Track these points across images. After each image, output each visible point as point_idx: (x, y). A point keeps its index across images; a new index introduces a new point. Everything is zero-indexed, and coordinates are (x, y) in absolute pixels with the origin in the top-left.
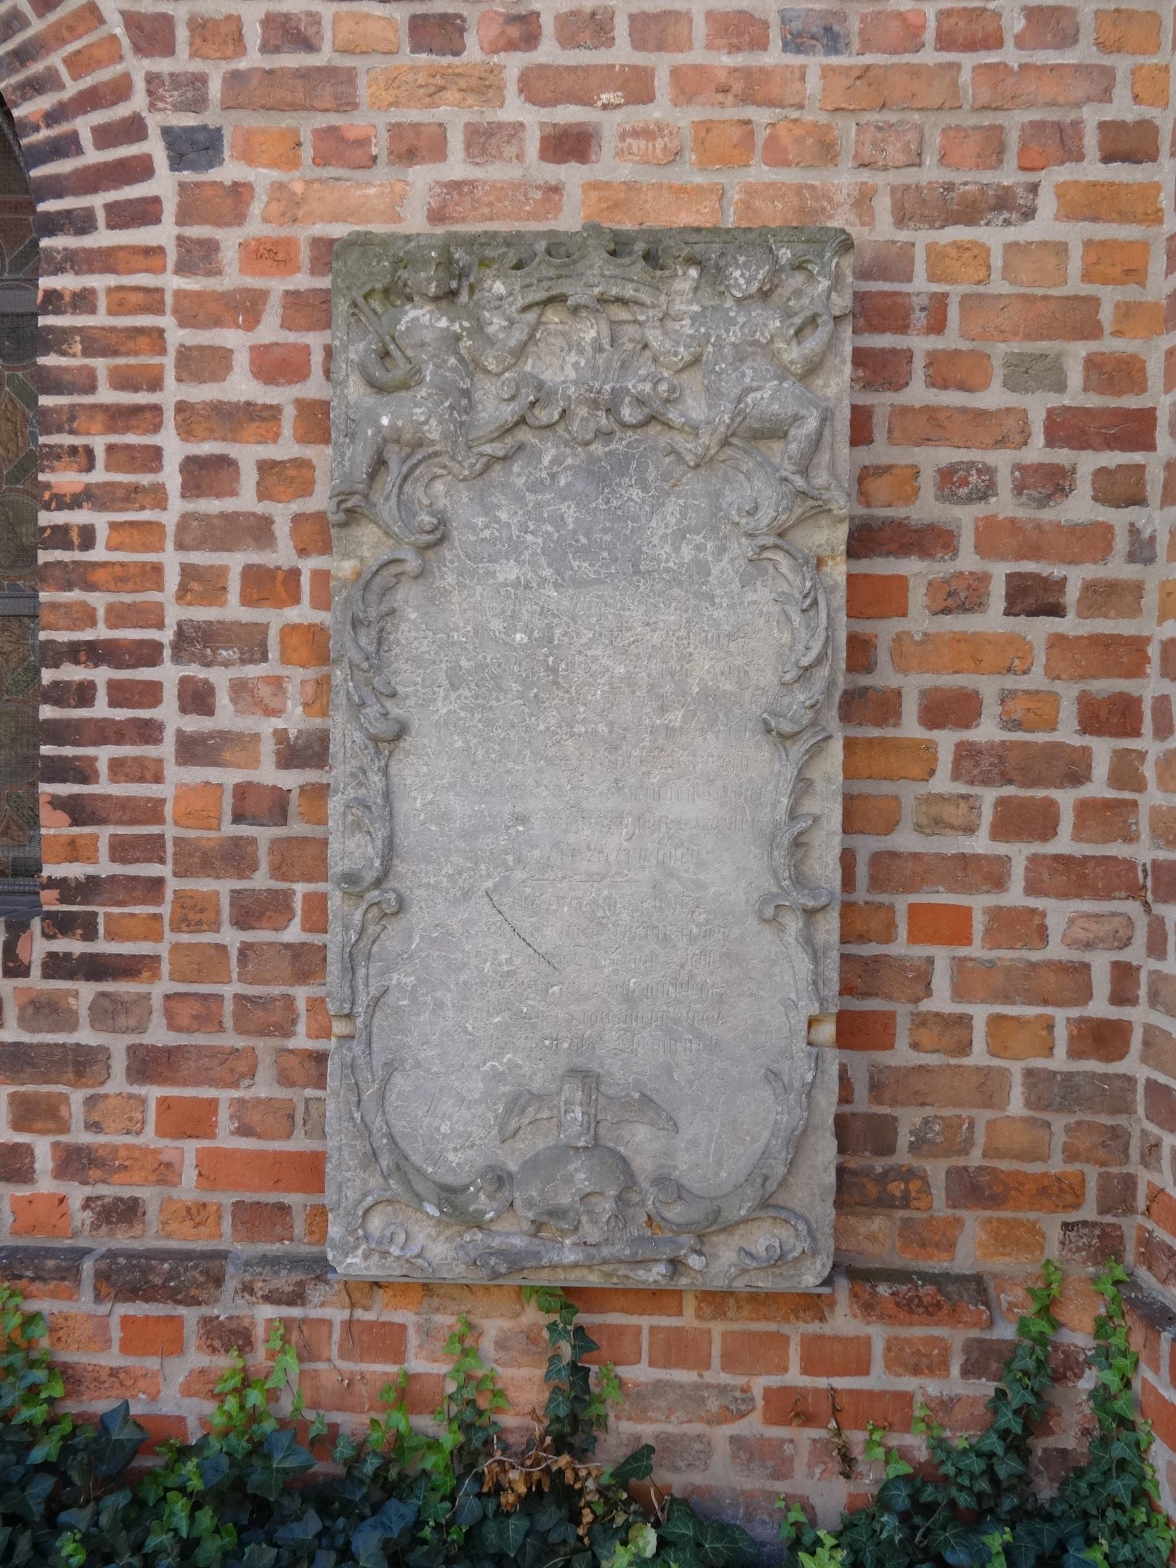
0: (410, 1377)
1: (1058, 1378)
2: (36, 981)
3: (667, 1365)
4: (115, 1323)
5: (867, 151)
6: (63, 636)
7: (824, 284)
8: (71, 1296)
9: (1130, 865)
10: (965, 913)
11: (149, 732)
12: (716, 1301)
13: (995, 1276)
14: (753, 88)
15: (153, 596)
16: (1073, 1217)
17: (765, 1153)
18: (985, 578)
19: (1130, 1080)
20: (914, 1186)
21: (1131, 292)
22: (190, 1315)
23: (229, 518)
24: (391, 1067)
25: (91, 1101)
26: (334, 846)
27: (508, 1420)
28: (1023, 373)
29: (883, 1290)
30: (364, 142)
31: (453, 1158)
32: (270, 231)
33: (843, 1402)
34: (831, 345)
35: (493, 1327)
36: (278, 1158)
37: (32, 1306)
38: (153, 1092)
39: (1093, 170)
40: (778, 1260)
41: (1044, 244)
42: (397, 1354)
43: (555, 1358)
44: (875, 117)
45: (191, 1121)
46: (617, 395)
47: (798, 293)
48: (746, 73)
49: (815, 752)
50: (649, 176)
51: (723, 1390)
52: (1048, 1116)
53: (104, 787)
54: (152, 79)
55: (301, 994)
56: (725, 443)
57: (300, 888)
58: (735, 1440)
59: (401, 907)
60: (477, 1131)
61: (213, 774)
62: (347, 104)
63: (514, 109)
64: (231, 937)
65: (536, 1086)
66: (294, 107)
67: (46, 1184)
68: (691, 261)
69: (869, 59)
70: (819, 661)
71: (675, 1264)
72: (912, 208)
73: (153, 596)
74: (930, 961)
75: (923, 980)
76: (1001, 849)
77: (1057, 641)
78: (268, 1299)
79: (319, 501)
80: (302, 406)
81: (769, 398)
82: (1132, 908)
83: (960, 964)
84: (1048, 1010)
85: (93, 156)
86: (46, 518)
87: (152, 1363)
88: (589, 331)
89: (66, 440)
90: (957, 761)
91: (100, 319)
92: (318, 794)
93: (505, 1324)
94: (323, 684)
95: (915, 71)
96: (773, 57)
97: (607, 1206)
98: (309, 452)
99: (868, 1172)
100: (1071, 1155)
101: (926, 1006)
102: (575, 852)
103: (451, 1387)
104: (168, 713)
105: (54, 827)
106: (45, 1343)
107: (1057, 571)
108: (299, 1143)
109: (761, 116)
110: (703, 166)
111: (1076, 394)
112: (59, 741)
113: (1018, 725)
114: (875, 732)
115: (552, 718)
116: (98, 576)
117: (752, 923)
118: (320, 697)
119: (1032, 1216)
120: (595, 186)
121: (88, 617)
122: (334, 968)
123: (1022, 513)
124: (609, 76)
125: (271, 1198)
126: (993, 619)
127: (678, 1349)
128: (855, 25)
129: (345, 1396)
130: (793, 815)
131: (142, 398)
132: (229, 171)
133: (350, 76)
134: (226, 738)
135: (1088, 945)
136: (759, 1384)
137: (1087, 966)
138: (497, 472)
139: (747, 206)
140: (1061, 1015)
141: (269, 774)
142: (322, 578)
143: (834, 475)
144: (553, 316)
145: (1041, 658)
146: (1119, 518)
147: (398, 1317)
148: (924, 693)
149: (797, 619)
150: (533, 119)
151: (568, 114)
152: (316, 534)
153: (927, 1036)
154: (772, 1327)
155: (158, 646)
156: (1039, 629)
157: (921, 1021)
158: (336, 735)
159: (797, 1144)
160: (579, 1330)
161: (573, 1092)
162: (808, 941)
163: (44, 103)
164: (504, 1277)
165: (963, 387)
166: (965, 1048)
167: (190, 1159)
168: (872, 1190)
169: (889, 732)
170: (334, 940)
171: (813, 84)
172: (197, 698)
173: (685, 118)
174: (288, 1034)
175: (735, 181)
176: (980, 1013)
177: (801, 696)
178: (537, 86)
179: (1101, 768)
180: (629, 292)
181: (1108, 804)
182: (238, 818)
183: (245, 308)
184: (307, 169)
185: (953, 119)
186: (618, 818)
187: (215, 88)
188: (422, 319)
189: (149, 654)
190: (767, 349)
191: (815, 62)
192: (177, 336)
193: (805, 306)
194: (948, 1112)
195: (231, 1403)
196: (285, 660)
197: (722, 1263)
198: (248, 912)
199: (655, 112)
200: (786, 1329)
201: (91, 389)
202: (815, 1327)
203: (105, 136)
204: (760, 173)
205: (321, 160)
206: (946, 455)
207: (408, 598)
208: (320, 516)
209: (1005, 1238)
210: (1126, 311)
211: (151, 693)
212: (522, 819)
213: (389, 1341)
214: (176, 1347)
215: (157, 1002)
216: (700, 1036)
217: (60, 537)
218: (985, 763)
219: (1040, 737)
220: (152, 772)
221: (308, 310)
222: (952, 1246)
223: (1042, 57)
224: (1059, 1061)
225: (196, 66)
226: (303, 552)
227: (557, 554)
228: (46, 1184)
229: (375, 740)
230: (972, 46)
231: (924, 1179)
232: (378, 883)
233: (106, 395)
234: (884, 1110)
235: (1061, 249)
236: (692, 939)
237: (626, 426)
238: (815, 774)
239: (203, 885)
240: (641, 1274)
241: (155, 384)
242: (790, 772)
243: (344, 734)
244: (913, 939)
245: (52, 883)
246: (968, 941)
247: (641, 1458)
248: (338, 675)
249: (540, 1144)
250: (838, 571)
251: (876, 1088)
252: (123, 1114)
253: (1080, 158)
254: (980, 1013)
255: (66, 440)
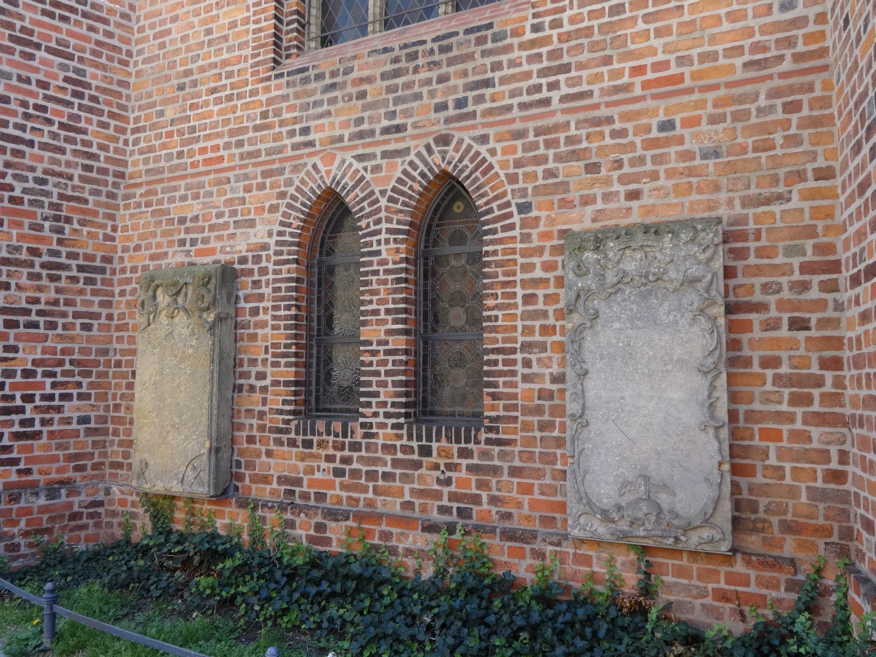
0: (594, 573)
1: (821, 595)
2: (482, 445)
3: (678, 577)
4: (506, 548)
5: (731, 186)
6: (490, 347)
7: (711, 235)
8: (494, 538)
9: (843, 415)
10: (780, 432)
11: (513, 373)
12: (694, 554)
13: (799, 560)
14: (691, 172)
15: (514, 334)
16: (829, 540)
17: (706, 505)
18: (780, 319)
19: (849, 492)
20: (766, 525)
21: (829, 222)
22: (527, 547)
23: (536, 311)
24: (586, 472)
25: (498, 482)
26: (568, 406)
27: (626, 590)
28: (789, 252)
29: (754, 558)
30: (572, 201)
31: (605, 501)
32: (546, 229)
33: (740, 595)
34: (715, 253)
35: (620, 559)
36: (552, 502)
37: (483, 540)
38: (516, 480)
39: (812, 184)
40: (711, 541)
41: (795, 210)
42: (590, 566)
43: (639, 568)
44: (733, 176)
45: (527, 490)
46: (647, 273)
47: (704, 238)
48: (689, 168)
49: (716, 377)
50: (658, 202)
51: (698, 587)
52: (817, 503)
53: (501, 389)
54: (513, 190)
55: (559, 452)
56: (682, 284)
57: (558, 420)
58: (702, 605)
59: (587, 424)
60: (612, 493)
61: (532, 386)
62: (567, 191)
63: (616, 187)
64: (538, 434)
65: (630, 479)
66: (552, 194)
67: (485, 506)
68: (668, 232)
69: (729, 159)
70: (715, 349)
71: (677, 539)
72: (746, 202)
73: (514, 334)
74: (768, 447)
75: (766, 454)
76: (792, 409)
77: (808, 339)
78: (550, 544)
79: (561, 305)
80: (556, 278)
81: (694, 271)
82: (845, 430)
83: (779, 449)
84: (814, 466)
85: (497, 213)
86: (485, 314)
87: (516, 561)
88: (638, 255)
89: (490, 291)
90: (774, 380)
91: (500, 257)
92: (562, 391)
93: (624, 558)
94: (564, 358)
95: (745, 160)
96: (698, 162)
97: (653, 518)
98: (558, 291)
99: (749, 519)
100: (827, 518)
101: (767, 462)
102: (639, 408)
103: (607, 577)
104: (519, 368)
105: (487, 401)
106: (486, 552)
107: (807, 316)
108: (559, 498)
109: (694, 180)
110: (676, 197)
111: (810, 257)
112: (489, 376)
113: (796, 367)
114: (743, 370)
115: (631, 368)
116: (500, 329)
117: (698, 431)
118: (563, 362)
119: (813, 539)
120: (642, 206)
121: (496, 341)
122: (568, 443)
123: (792, 297)
124: (645, 174)
125: (551, 515)
126: (784, 332)
127: (681, 572)
128: (724, 149)
129: (574, 576)
130: (709, 396)
131: (511, 278)
132: (534, 213)
133: (568, 183)
134: (536, 375)
135: (828, 443)
136: (710, 586)
137: (828, 451)
138: (612, 297)
139: (691, 209)
140: (819, 468)
141: (548, 385)
142: (563, 327)
143: (718, 292)
144: (628, 252)
145: (803, 345)
146: (830, 297)
147: (590, 553)
148: (761, 357)
149: (708, 336)
150: (622, 189)
151: (633, 187)
152: (560, 315)
153: (768, 473)
154: (714, 567)
155: (516, 349)
156: (802, 335)
157: (766, 468)
158: (568, 374)
159: (717, 502)
160: (647, 561)
161: (641, 481)
162: (717, 437)
163: (484, 200)
164: (622, 541)
165: (768, 257)
166: (783, 477)
167: (526, 501)
168: (751, 525)
169: (748, 370)
170: (568, 435)
171: (711, 168)
172: (527, 363)
173: (670, 183)
174: (555, 464)
175: (687, 200)
176: (788, 466)
177: (710, 360)
178: (623, 180)
179: (829, 381)
180: (650, 243)
181: (832, 394)
182: (539, 399)
183: (540, 251)
184: (556, 210)
185: (759, 173)
186: (652, 398)
187: (530, 191)
188: (589, 256)
189: (513, 351)
190: (694, 256)
191: (711, 162)
192: (520, 261)
193: (706, 242)
194: (778, 500)
195: (540, 574)
196: (552, 352)
197: (693, 540)
198: (544, 426)
199: (661, 183)
200: (719, 568)
201: (497, 277)
202: (729, 569)
203: (500, 207)
204: (695, 197)
205: (560, 207)
206: (764, 280)
207: (587, 334)
208: (562, 309)
209: (802, 546)
210: (827, 228)
211: (514, 362)
212: (623, 398)
213: (587, 561)
214: (523, 557)
215: (516, 453)
216: (682, 466)
217: (489, 319)
218: (784, 380)
219: (805, 371)
220: (514, 385)
221: (557, 250)
222: (782, 547)
223: (790, 151)
224: (819, 484)
225: (524, 185)
226: (557, 320)
227: (631, 320)
228: (485, 506)
229: (579, 375)
230: (765, 150)
231: (770, 523)
232: (581, 417)
233: (501, 278)
234: (754, 498)
235: (801, 210)
236: (678, 435)
237: (650, 282)
238: (716, 384)
239: (530, 418)
240: (665, 541)
241: (514, 274)
242: (708, 384)
243: (570, 374)
244: (761, 439)
245: (487, 417)
246: (782, 441)
247: (668, 606)
248: (568, 356)
249: (632, 498)
250: (722, 321)
251: (751, 490)
252: (507, 486)
253: (807, 180)
254: (788, 466)
255: (490, 291)
